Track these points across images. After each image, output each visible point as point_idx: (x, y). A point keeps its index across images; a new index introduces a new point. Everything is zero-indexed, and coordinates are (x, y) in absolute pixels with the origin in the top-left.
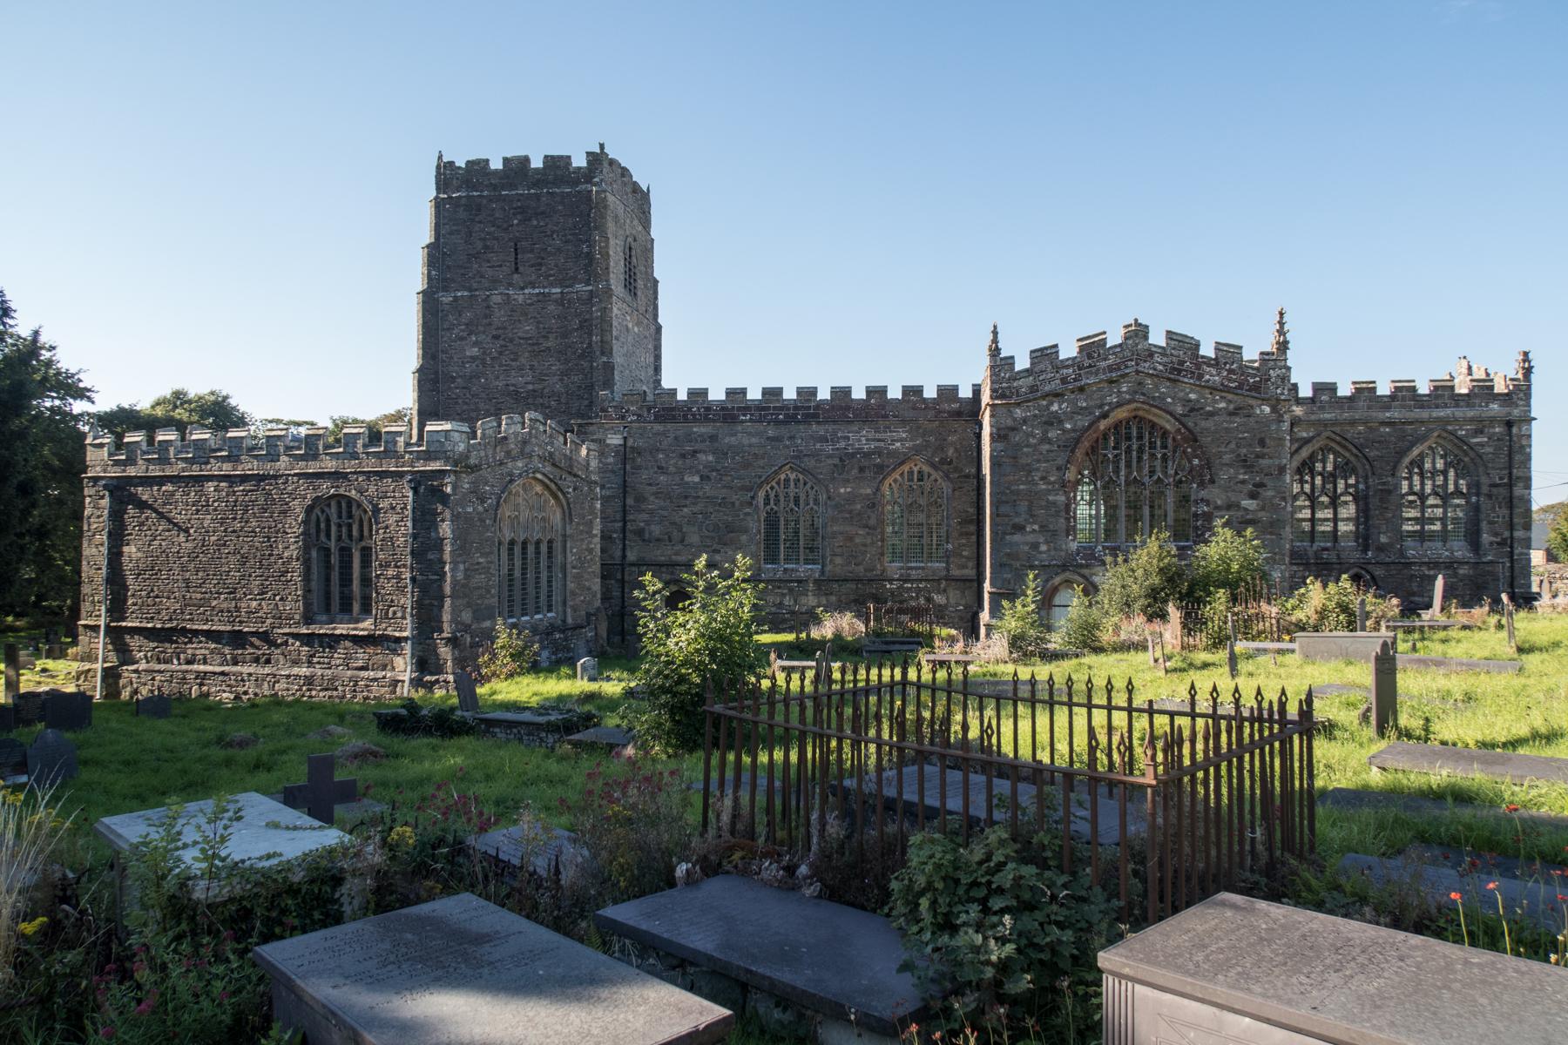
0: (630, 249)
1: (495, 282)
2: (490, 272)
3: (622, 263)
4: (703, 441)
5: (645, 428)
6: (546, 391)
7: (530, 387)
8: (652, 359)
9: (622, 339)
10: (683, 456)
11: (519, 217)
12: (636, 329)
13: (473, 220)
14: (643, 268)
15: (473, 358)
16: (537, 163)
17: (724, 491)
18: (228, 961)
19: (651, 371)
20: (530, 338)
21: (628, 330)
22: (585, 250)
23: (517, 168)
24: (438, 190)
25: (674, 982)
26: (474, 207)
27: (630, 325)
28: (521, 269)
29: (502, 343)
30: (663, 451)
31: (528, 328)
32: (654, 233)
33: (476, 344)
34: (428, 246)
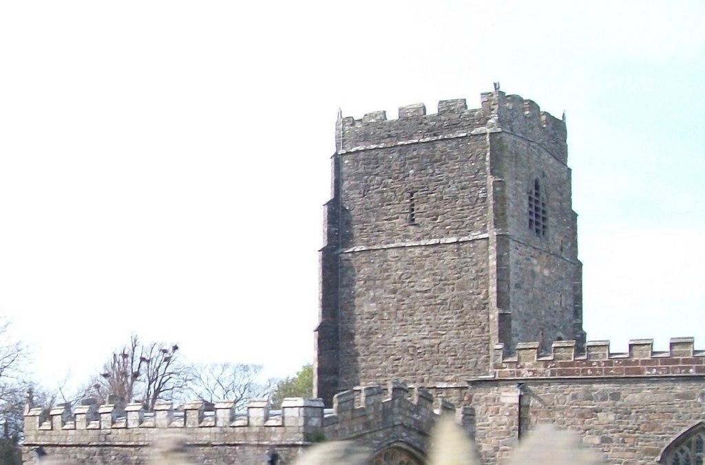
0: (537, 187)
1: (392, 234)
2: (387, 225)
3: (526, 202)
4: (604, 399)
5: (606, 374)
6: (442, 345)
7: (427, 342)
8: (570, 301)
9: (525, 286)
10: (582, 416)
11: (415, 166)
12: (546, 272)
13: (370, 174)
14: (555, 204)
15: (373, 315)
16: (432, 110)
17: (629, 454)
18: (329, 405)
19: (568, 316)
20: (426, 292)
21: (533, 274)
22: (481, 196)
23: (413, 120)
24: (337, 145)
25: (335, 440)
26: (371, 160)
27: (537, 269)
28: (417, 220)
29: (399, 297)
30: (561, 410)
31: (426, 282)
32: (570, 163)
33: (373, 300)
34: (328, 204)
